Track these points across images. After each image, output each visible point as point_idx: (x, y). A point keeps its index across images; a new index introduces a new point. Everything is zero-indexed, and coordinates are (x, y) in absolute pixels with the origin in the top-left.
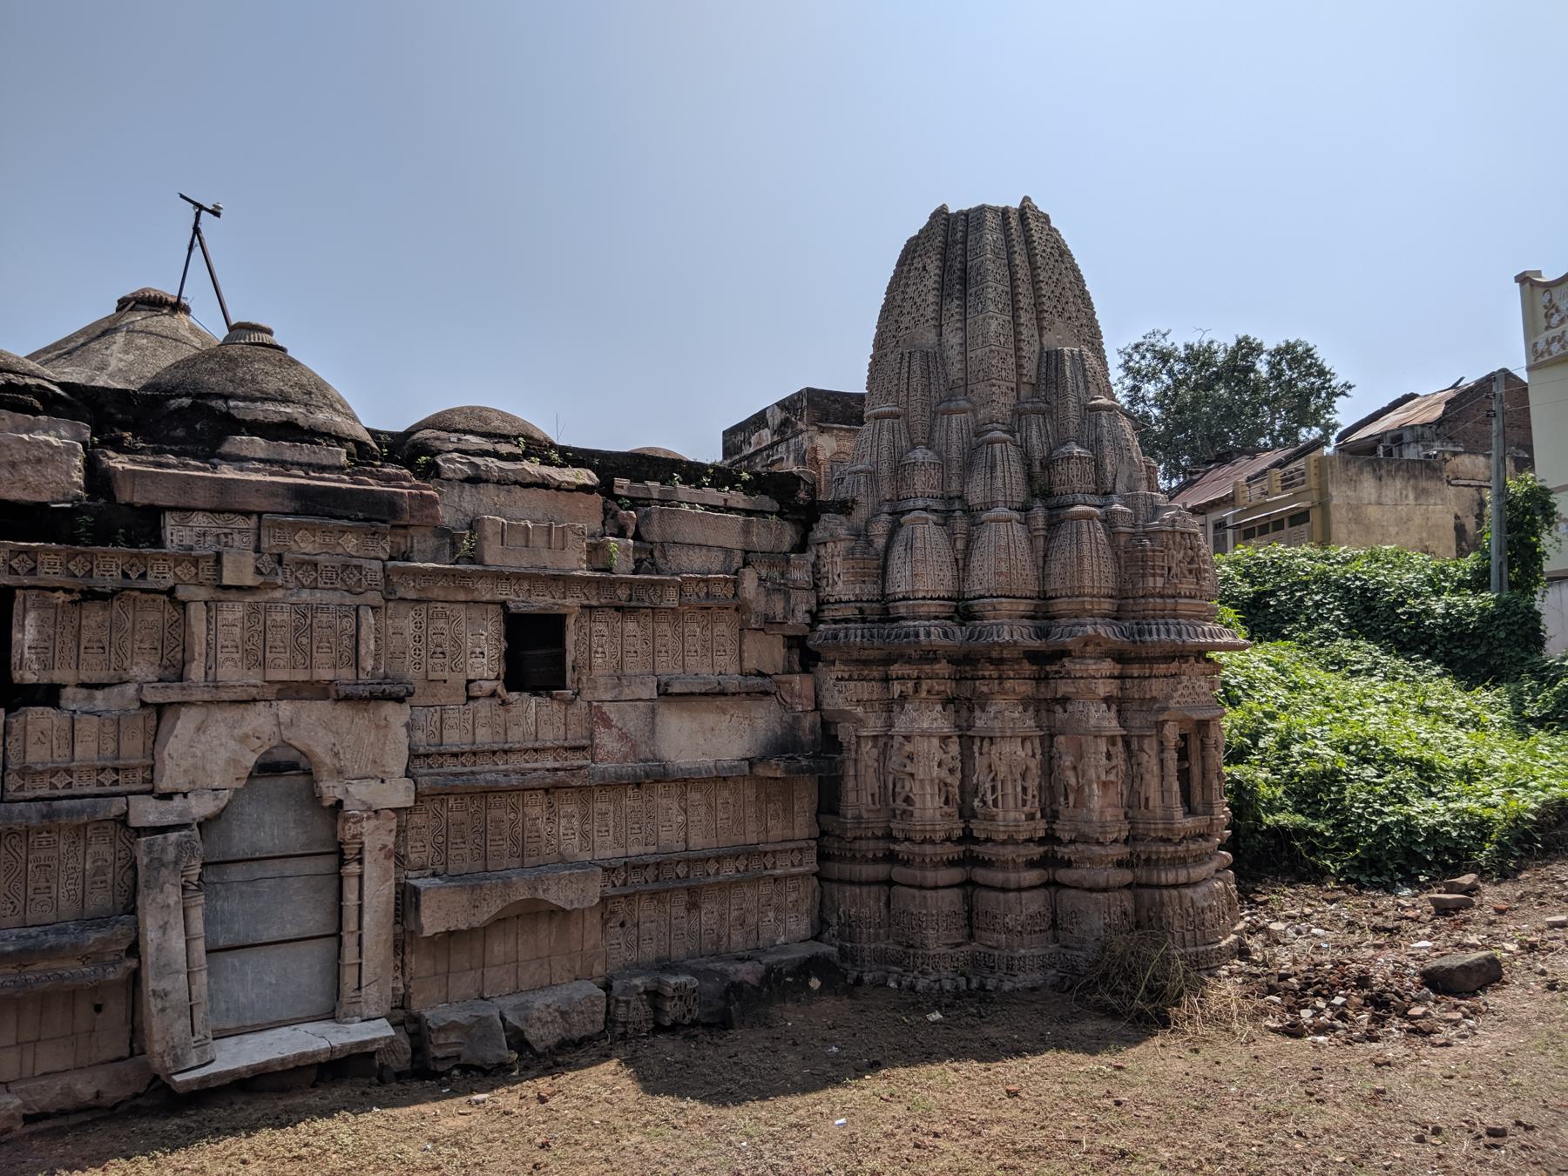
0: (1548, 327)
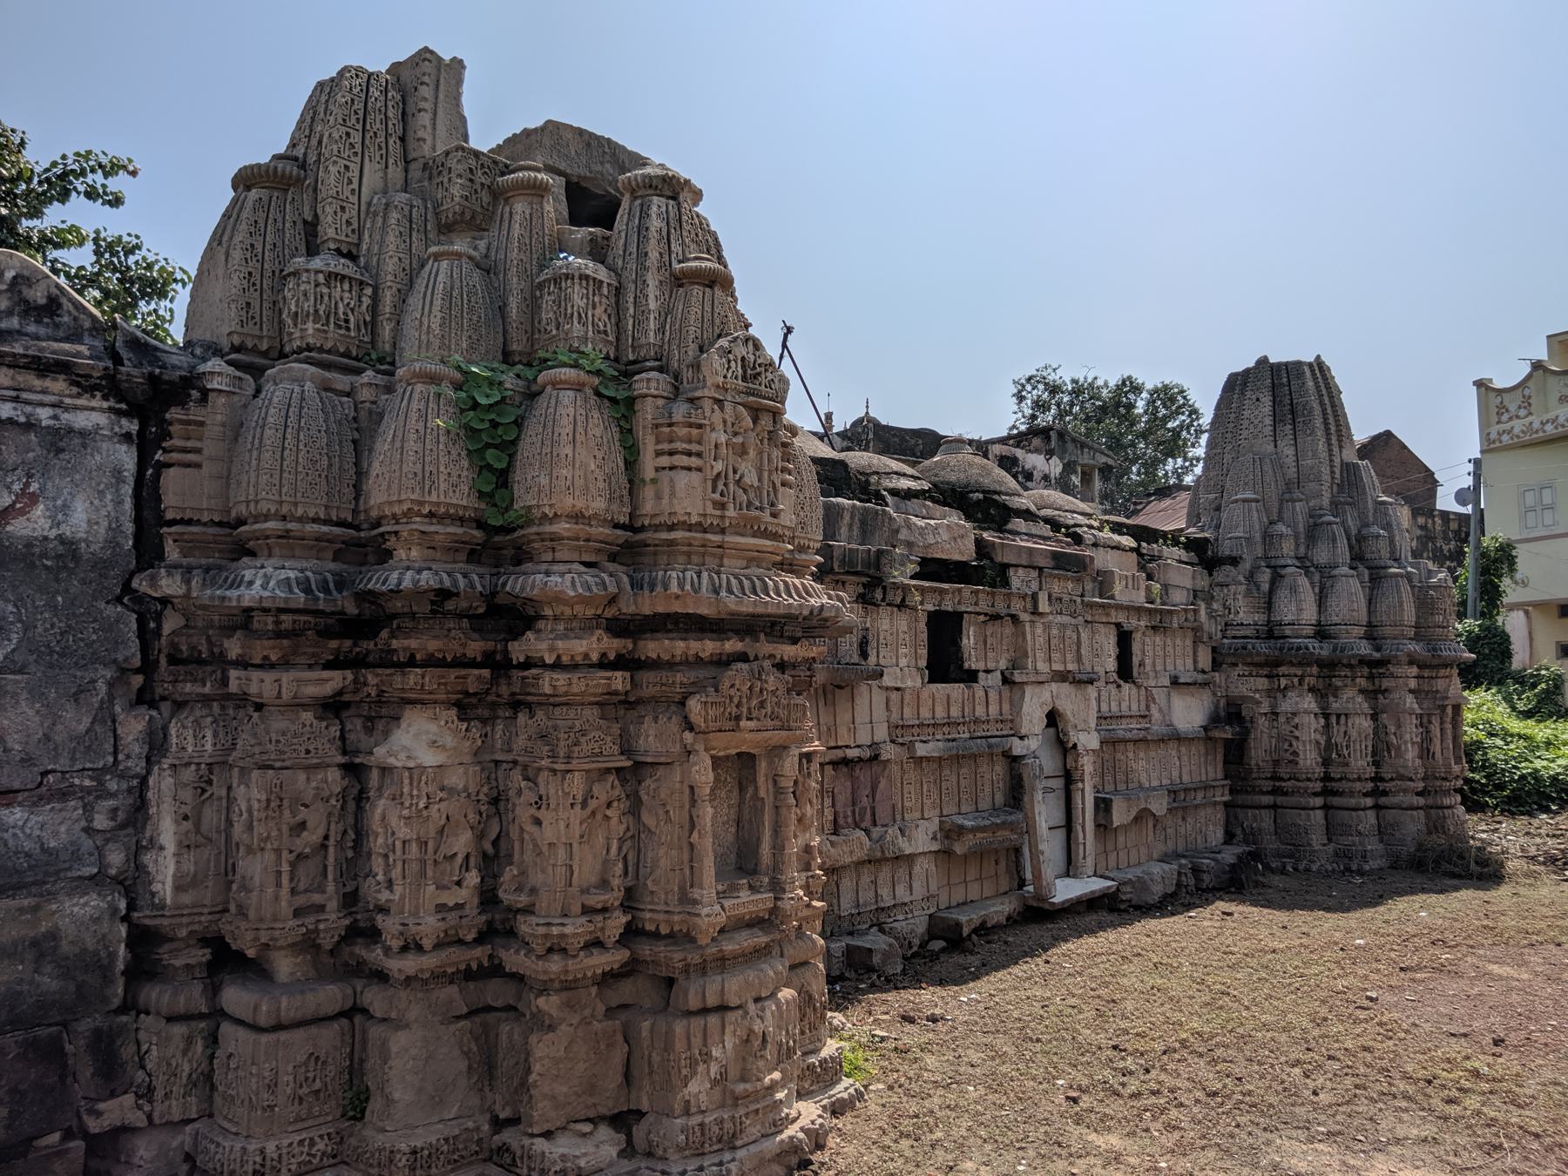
0: (1499, 422)
